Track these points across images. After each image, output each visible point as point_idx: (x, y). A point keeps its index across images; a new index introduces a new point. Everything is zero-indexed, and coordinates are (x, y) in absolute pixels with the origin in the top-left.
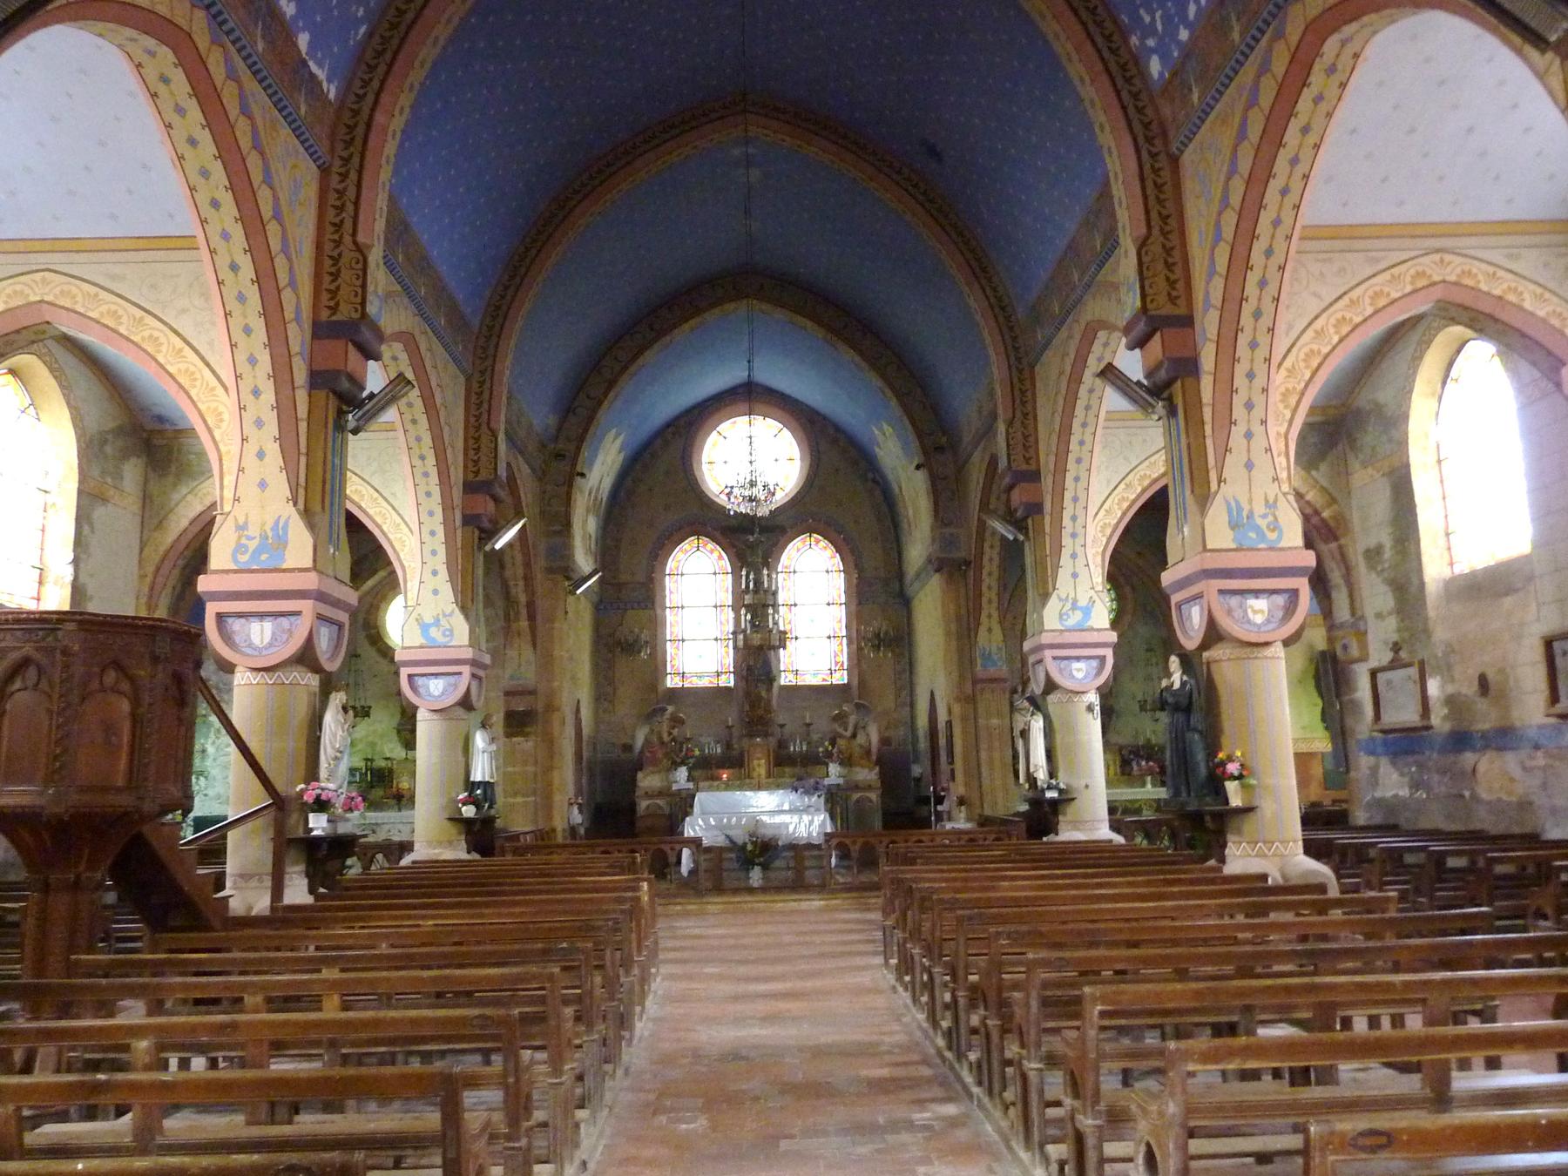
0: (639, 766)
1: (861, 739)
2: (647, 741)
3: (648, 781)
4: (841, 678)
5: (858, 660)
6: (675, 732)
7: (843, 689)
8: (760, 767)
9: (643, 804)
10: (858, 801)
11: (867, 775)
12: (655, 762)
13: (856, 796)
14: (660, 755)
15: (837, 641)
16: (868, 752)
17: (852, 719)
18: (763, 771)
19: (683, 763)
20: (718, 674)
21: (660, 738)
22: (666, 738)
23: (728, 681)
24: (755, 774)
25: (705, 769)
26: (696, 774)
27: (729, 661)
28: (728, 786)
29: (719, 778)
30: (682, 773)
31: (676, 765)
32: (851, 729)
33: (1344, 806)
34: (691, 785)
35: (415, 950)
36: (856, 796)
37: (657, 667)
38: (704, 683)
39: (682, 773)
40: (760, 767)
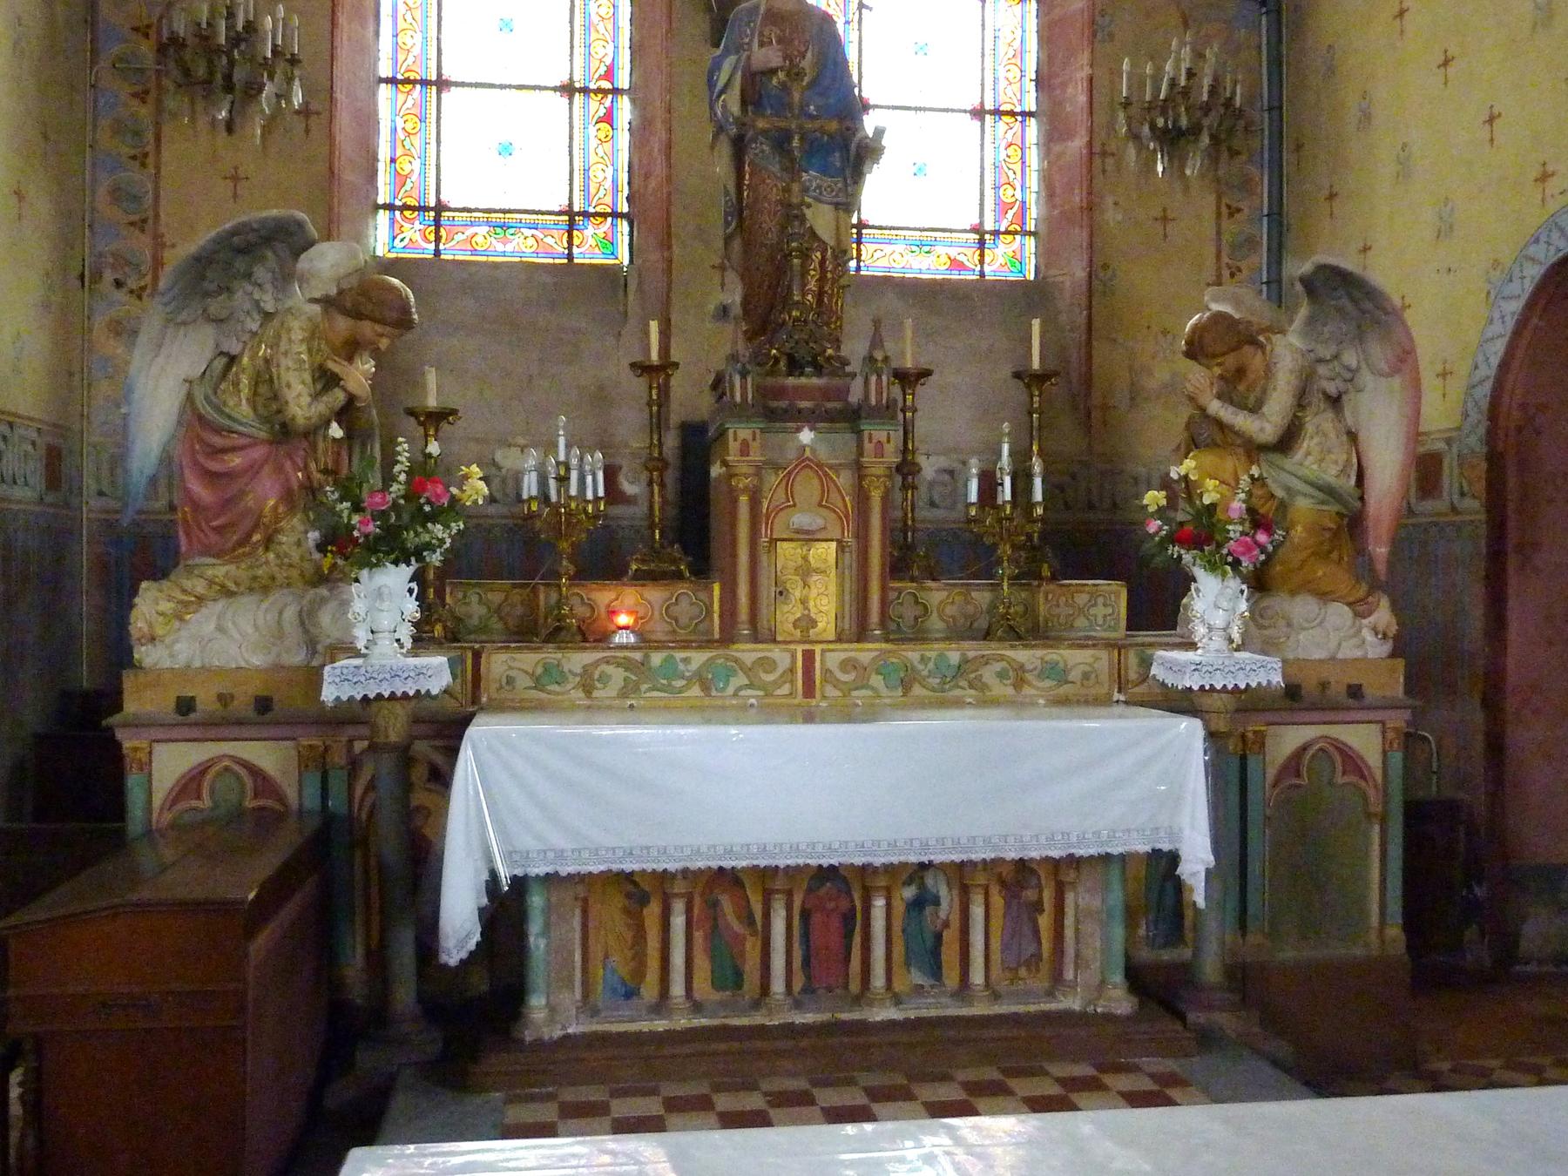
0: (146, 553)
1: (1317, 459)
2: (200, 425)
3: (196, 635)
4: (1013, 260)
5: (1079, 201)
6: (359, 374)
7: (1026, 298)
8: (811, 578)
9: (165, 766)
10: (1293, 764)
11: (1345, 635)
12: (241, 536)
13: (1289, 739)
14: (266, 495)
15: (1002, 130)
16: (1352, 523)
17: (1288, 350)
18: (823, 601)
19: (389, 545)
20: (572, 218)
21: (267, 387)
22: (301, 403)
23: (606, 245)
24: (787, 615)
25: (517, 585)
26: (474, 603)
27: (609, 166)
28: (642, 692)
29: (592, 634)
30: (384, 601)
31: (346, 552)
32: (1278, 406)
33: (118, 516)
34: (435, 673)
35: (1264, 58)
36: (1289, 739)
37: (337, 176)
38: (520, 247)
39: (384, 601)
40: (811, 578)
